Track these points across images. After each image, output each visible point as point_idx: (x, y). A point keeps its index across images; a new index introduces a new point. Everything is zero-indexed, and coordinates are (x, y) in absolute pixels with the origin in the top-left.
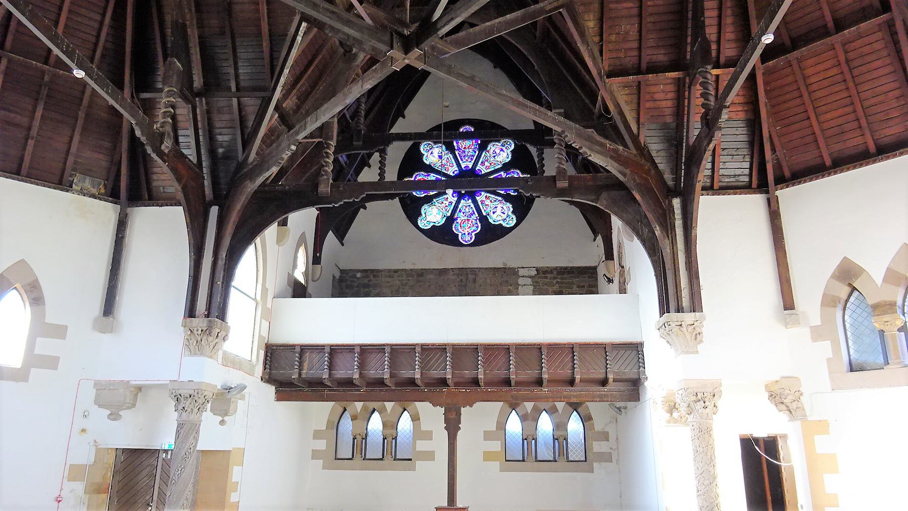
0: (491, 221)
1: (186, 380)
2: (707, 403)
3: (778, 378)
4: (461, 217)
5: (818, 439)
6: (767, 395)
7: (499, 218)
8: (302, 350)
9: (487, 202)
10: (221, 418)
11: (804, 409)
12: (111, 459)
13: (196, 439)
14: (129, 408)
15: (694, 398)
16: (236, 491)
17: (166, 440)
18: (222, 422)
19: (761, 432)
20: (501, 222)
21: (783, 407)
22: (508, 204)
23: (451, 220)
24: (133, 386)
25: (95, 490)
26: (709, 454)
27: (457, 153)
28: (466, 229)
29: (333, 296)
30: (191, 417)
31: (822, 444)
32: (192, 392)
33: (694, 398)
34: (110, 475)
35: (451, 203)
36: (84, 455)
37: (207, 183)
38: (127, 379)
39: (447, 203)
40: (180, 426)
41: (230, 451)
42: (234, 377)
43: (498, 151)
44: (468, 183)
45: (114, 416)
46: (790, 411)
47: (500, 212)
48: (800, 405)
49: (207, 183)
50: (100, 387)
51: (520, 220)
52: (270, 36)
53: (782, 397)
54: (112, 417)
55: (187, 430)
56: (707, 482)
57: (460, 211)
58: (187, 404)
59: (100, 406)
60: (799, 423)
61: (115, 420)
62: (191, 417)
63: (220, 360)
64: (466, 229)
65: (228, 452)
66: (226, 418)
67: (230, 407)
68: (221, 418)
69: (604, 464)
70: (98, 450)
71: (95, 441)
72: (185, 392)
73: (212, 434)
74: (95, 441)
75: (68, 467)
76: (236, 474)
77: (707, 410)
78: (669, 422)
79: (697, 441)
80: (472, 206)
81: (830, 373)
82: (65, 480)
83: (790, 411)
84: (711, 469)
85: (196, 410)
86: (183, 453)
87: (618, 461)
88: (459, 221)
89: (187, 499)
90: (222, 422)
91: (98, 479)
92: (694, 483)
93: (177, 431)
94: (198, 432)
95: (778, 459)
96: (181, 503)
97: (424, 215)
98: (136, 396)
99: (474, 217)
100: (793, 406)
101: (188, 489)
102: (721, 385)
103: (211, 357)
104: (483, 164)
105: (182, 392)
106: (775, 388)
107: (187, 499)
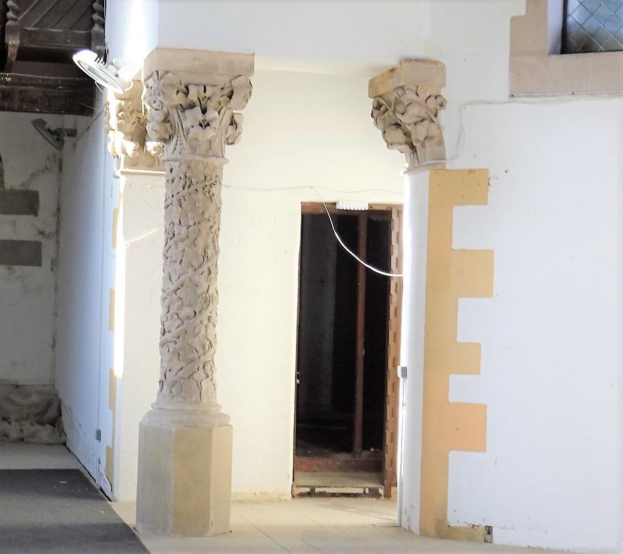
2: (212, 114)
3: (393, 62)
5: (461, 214)
6: (370, 104)
11: (441, 142)
15: (179, 99)
19: (354, 201)
21: (398, 135)
26: (201, 242)
29: (302, 213)
31: (469, 229)
33: (179, 99)
46: (413, 148)
48: (434, 130)
52: (438, 159)
53: (403, 110)
56: (187, 311)
60: (425, 175)
69: (19, 269)
77: (210, 133)
78: (133, 162)
79: (176, 209)
81: (513, 54)
83: (413, 148)
84: (202, 280)
87: (55, 263)
92: (158, 310)
95: (387, 269)
100: (419, 133)
102: (251, 69)
106: (386, 88)
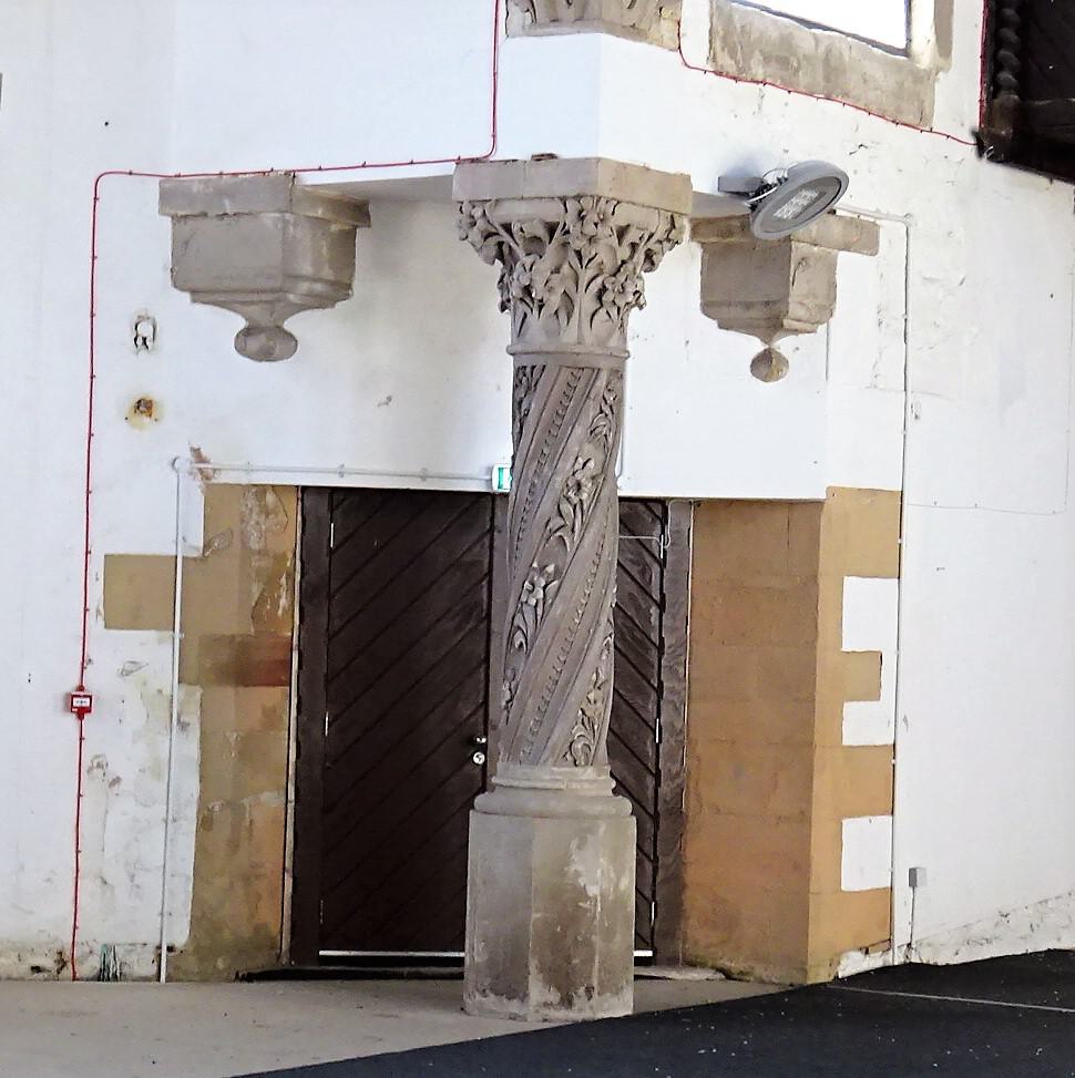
1: (523, 153)
10: (756, 346)
12: (285, 535)
13: (608, 444)
14: (322, 302)
16: (873, 694)
17: (484, 458)
18: (766, 365)
24: (316, 195)
25: (228, 666)
30: (569, 335)
32: (553, 212)
34: (286, 602)
36: (160, 519)
38: (283, 164)
40: (526, 380)
41: (818, 504)
42: (787, 131)
45: (266, 341)
50: (197, 207)
54: (254, 344)
55: (566, 396)
58: (539, 270)
59: (198, 295)
61: (265, 355)
62: (569, 335)
63: (696, 44)
65: (801, 512)
66: (784, 345)
67: (786, 283)
68: (756, 346)
70: (219, 498)
71: (198, 455)
72: (525, 214)
73: (693, 414)
74: (198, 455)
75: (97, 566)
76: (862, 613)
82: (96, 624)
85: (585, 301)
86: (547, 506)
89: (587, 722)
90: (766, 365)
91: (231, 621)
93: (517, 404)
94: (613, 409)
96: (559, 736)
98: (348, 238)
101: (586, 676)
103: (634, 32)
105: (512, 212)
107: (587, 722)
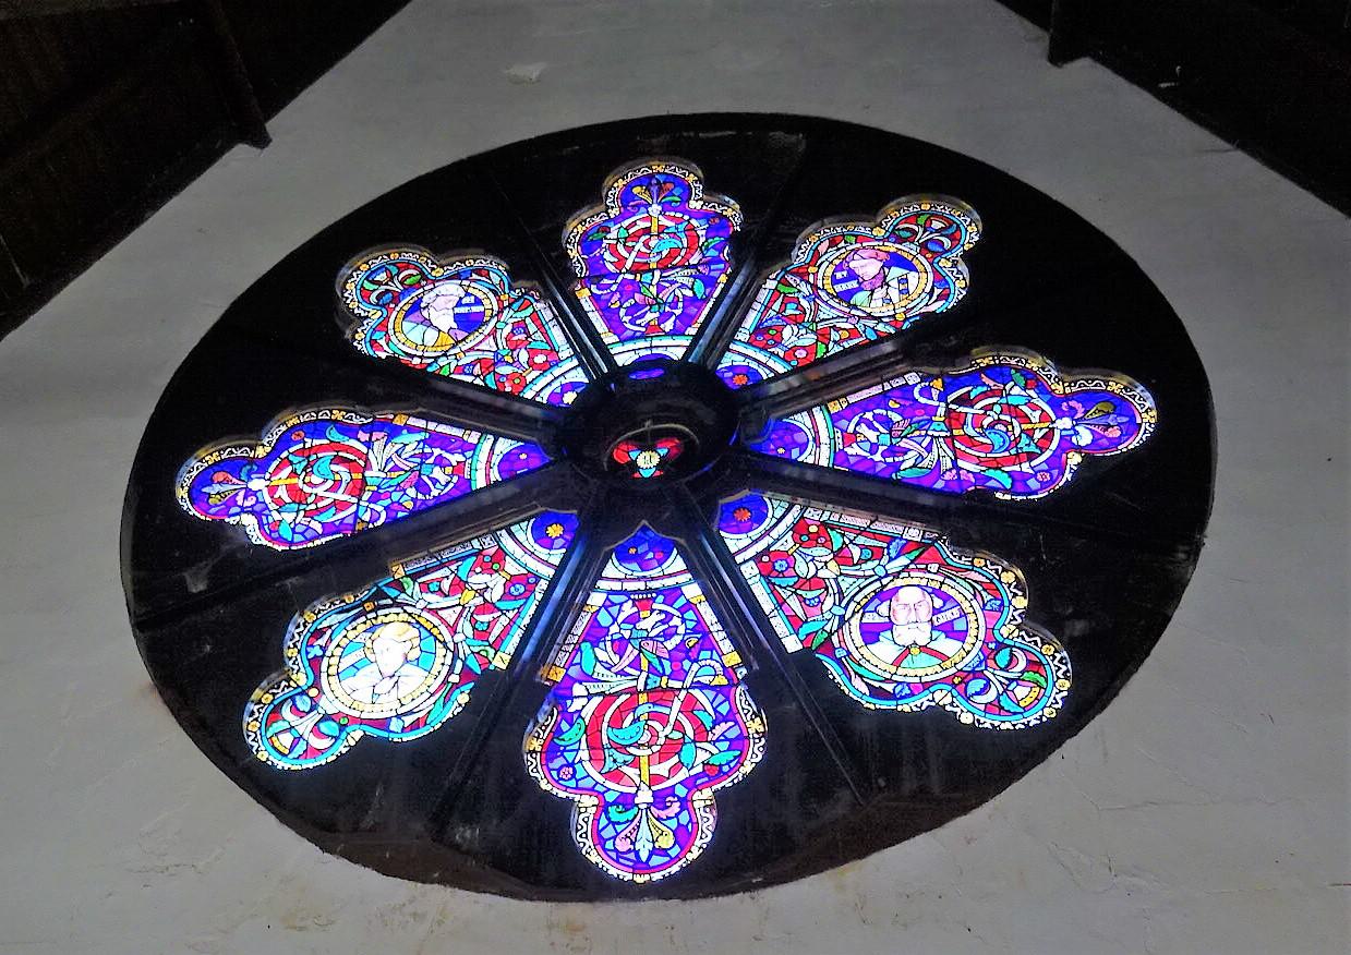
0: (857, 690)
4: (597, 675)
7: (921, 668)
8: (593, 748)
9: (815, 562)
20: (942, 696)
22: (983, 567)
23: (507, 701)
27: (584, 295)
28: (645, 761)
35: (528, 580)
37: (560, 298)
39: (496, 585)
43: (868, 267)
44: (658, 461)
47: (923, 635)
49: (560, 298)
51: (1104, 664)
57: (595, 634)
64: (645, 761)
80: (693, 592)
88: (582, 703)
97: (302, 679)
99: (705, 670)
104: (764, 336)
